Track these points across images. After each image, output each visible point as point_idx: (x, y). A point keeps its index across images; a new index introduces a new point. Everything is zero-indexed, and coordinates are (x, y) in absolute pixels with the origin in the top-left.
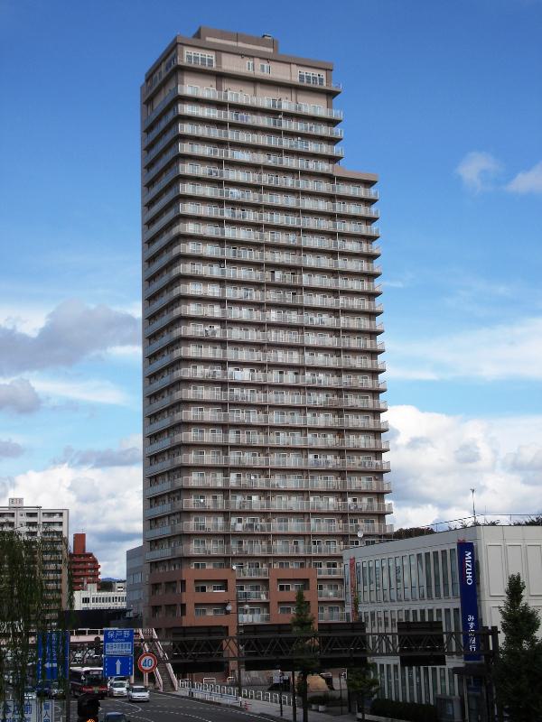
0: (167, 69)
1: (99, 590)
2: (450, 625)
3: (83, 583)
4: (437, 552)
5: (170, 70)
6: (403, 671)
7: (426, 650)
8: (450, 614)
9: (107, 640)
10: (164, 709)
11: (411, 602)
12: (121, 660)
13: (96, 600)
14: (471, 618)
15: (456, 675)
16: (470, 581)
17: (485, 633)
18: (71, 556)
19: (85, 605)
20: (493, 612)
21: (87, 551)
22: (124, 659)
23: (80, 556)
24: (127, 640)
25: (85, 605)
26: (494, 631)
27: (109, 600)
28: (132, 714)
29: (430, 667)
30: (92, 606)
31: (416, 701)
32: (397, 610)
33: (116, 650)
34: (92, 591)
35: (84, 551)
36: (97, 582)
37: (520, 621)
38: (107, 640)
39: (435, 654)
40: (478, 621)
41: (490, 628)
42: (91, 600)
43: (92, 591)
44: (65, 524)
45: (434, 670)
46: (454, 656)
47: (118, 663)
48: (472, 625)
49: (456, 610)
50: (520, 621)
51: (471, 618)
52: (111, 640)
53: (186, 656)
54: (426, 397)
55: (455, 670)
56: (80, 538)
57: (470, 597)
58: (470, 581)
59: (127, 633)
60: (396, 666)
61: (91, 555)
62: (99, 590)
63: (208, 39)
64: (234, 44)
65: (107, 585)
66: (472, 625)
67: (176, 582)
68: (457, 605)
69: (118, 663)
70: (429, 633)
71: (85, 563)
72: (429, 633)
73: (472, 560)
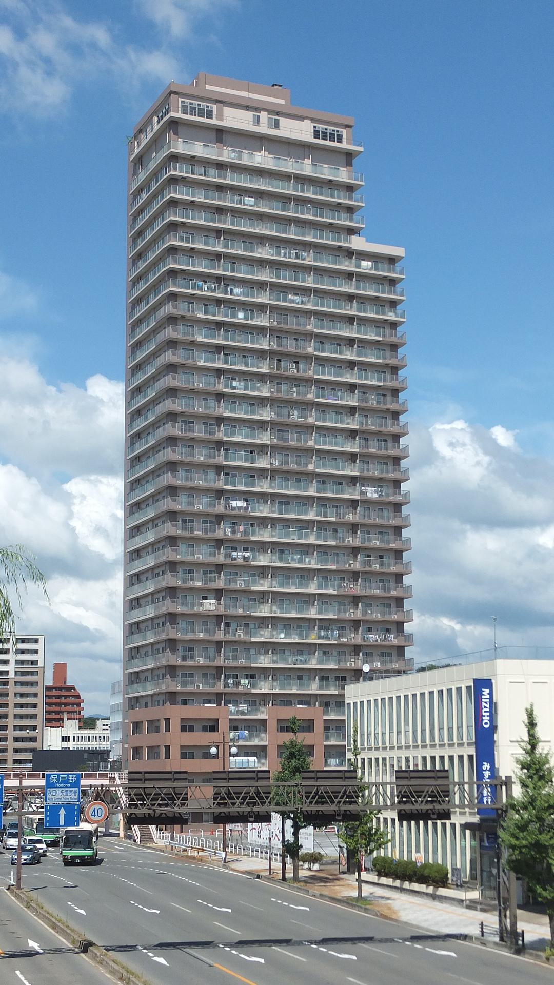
1: (80, 728)
2: (460, 774)
3: (62, 720)
4: (424, 693)
5: (162, 122)
6: (401, 825)
7: (427, 802)
9: (49, 785)
13: (77, 739)
14: (486, 766)
15: (468, 832)
16: (486, 724)
17: (499, 784)
18: (48, 688)
19: (65, 745)
20: (508, 760)
21: (69, 683)
22: (69, 807)
23: (60, 689)
24: (72, 785)
25: (65, 745)
26: (508, 782)
27: (89, 739)
29: (439, 822)
31: (431, 861)
32: (398, 757)
33: (57, 796)
34: (71, 728)
35: (65, 682)
36: (80, 720)
37: (535, 768)
38: (49, 785)
40: (493, 769)
41: (504, 778)
42: (71, 739)
43: (71, 728)
44: (41, 652)
45: (444, 825)
47: (62, 812)
48: (487, 774)
50: (535, 768)
51: (486, 766)
54: (76, 566)
55: (465, 826)
57: (485, 741)
58: (486, 724)
59: (72, 778)
60: (393, 820)
62: (80, 728)
63: (208, 87)
66: (487, 774)
67: (159, 720)
68: (472, 751)
69: (62, 812)
71: (66, 697)
73: (491, 699)
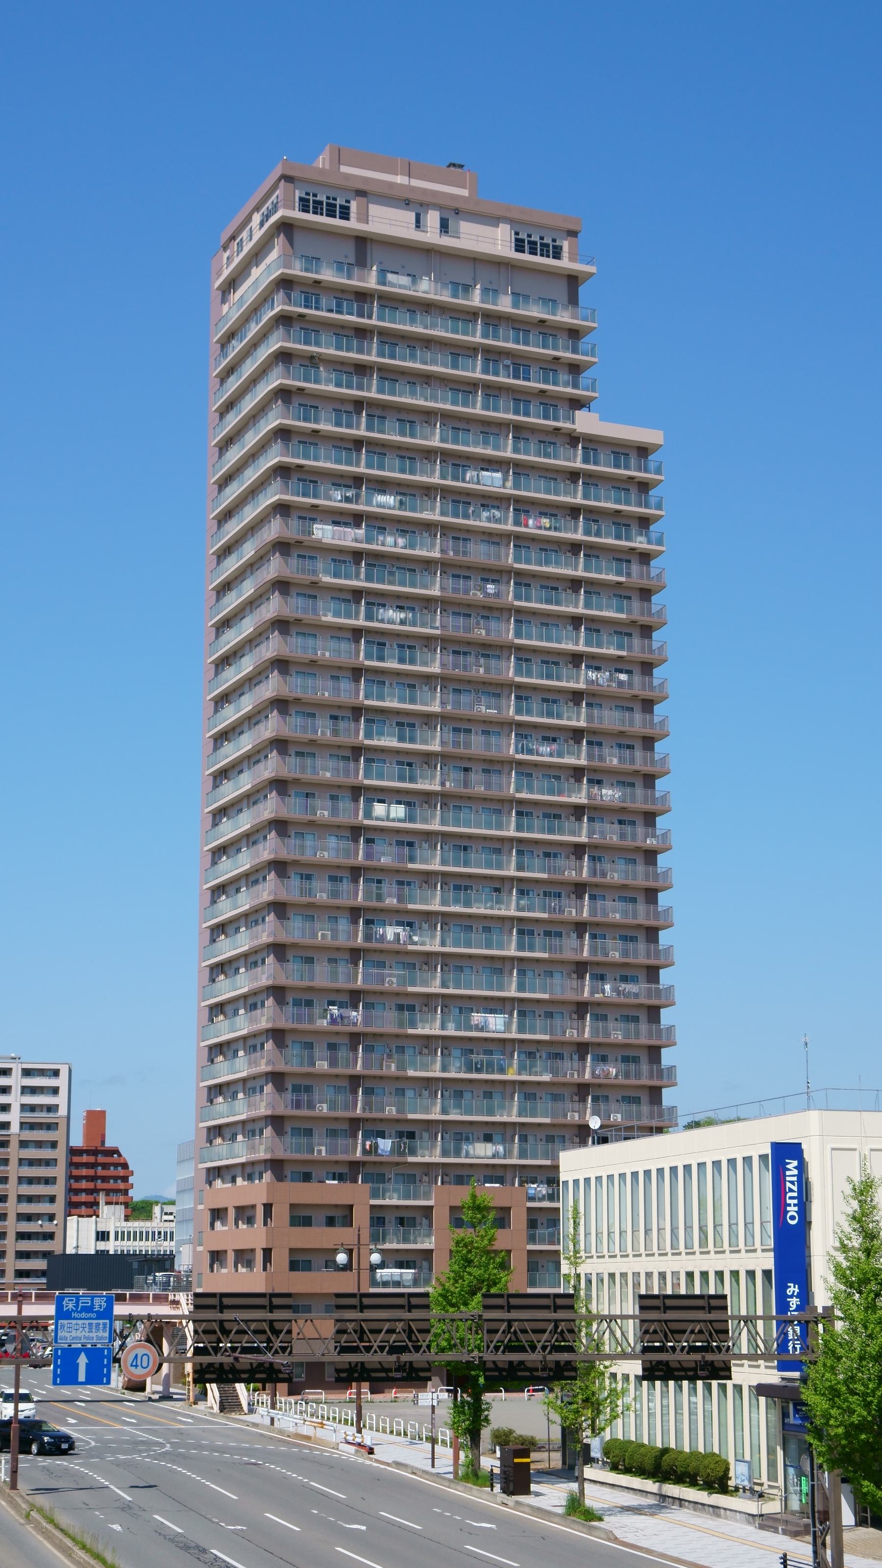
0: (262, 224)
2: (749, 1301)
8: (738, 1281)
9: (62, 1314)
10: (202, 1447)
11: (595, 1259)
12: (88, 1352)
14: (793, 1289)
16: (792, 1218)
18: (73, 1152)
21: (109, 1143)
24: (100, 1315)
28: (148, 1456)
30: (111, 1246)
33: (79, 1334)
35: (103, 1142)
36: (126, 1205)
39: (709, 1357)
42: (112, 1236)
43: (111, 1217)
44: (64, 1092)
46: (761, 1362)
47: (83, 1360)
48: (794, 1302)
49: (767, 1273)
52: (67, 1315)
53: (216, 1350)
56: (96, 1120)
58: (792, 1218)
61: (116, 1151)
64: (400, 179)
65: (139, 1210)
66: (794, 1302)
68: (768, 1261)
69: (83, 1360)
70: (407, 1315)
72: (407, 1315)
